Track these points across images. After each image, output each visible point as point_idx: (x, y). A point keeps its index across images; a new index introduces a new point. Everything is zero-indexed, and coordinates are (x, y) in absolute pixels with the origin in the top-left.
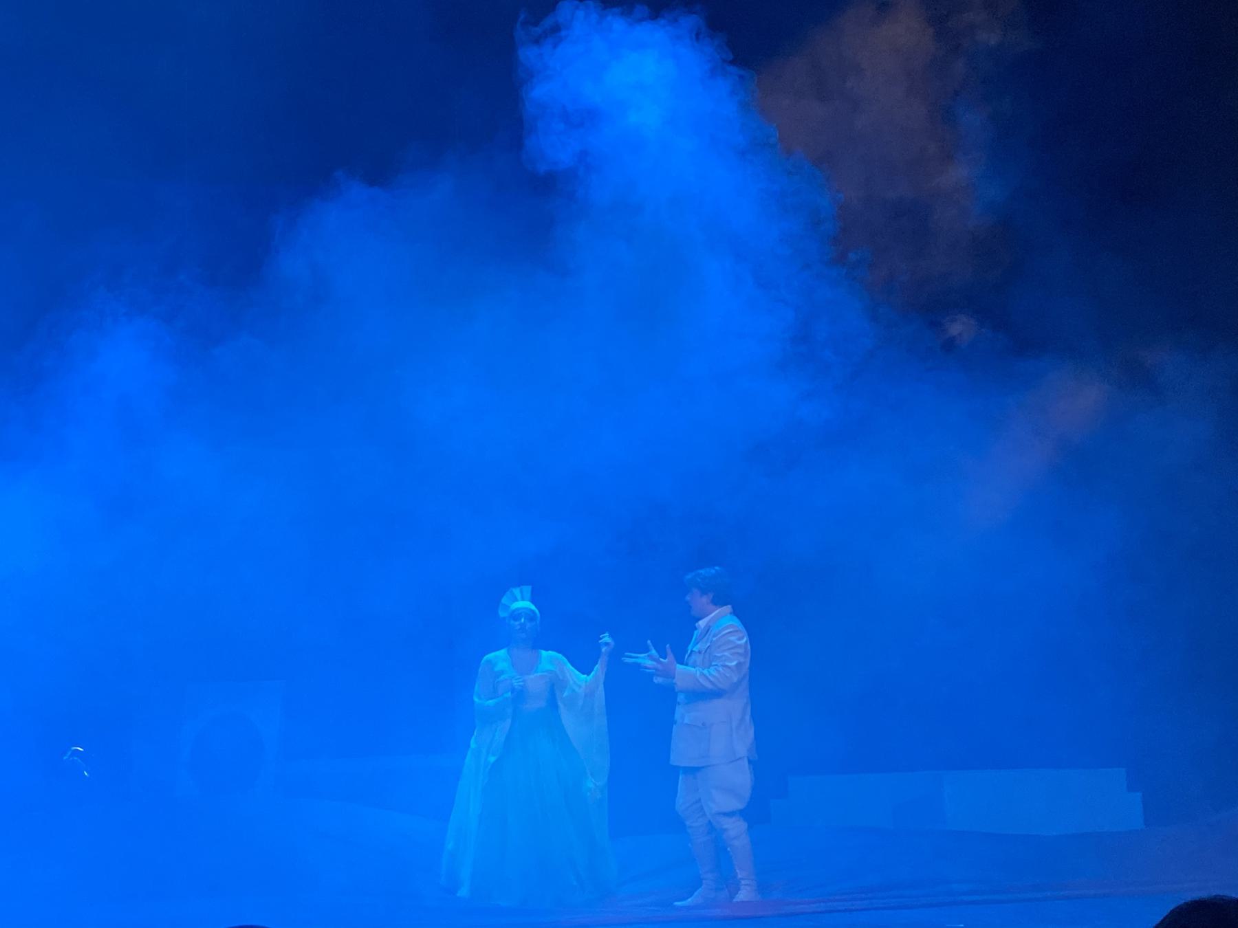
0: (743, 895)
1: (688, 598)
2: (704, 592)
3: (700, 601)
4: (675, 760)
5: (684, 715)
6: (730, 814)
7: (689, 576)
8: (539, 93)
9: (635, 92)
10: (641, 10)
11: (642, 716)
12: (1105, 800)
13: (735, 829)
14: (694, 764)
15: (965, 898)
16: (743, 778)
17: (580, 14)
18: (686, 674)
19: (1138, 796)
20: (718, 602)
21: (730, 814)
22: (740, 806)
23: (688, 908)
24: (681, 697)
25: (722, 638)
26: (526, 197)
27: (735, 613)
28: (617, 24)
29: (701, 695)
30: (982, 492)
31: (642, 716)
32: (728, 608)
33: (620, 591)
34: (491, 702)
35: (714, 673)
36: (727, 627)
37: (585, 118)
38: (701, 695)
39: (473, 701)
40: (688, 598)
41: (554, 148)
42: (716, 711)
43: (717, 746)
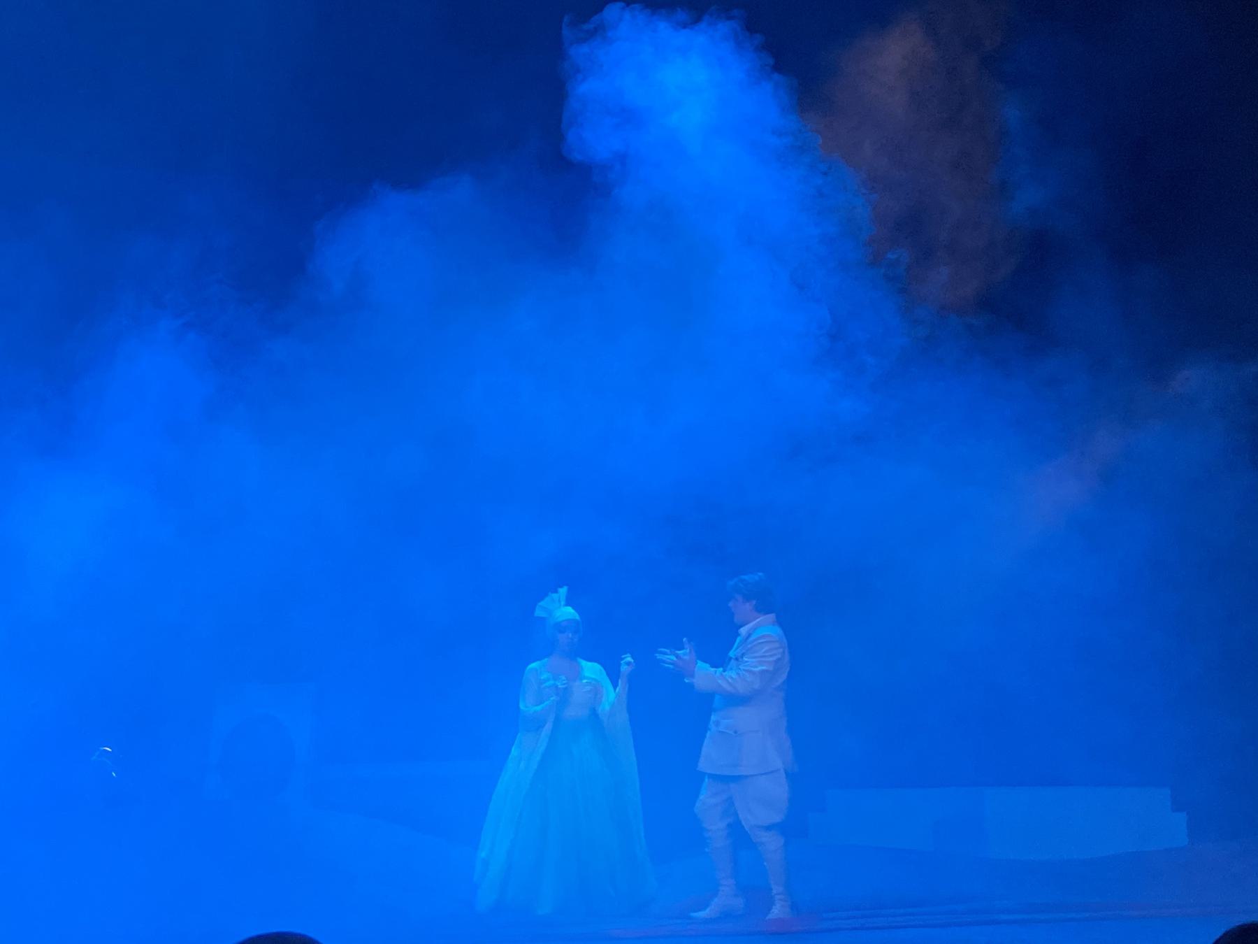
0: (778, 911)
1: (730, 604)
2: (747, 598)
3: (742, 608)
4: (703, 765)
5: (720, 721)
6: (768, 828)
7: (731, 583)
8: (586, 89)
9: (678, 96)
10: (681, 15)
11: (670, 721)
12: (1138, 820)
13: (772, 843)
14: (727, 772)
15: (1004, 917)
16: (779, 790)
17: (627, 16)
18: (704, 675)
19: (1182, 817)
20: (763, 608)
21: (768, 828)
22: (777, 818)
23: (706, 921)
24: (717, 701)
25: (761, 642)
26: (559, 191)
27: (779, 622)
28: (663, 28)
29: (736, 700)
30: (1010, 508)
31: (670, 721)
32: (772, 617)
33: (656, 596)
34: (538, 708)
35: (734, 676)
36: (763, 637)
37: (629, 117)
38: (736, 700)
39: (518, 708)
40: (730, 604)
41: (594, 140)
42: (743, 718)
43: (749, 752)
